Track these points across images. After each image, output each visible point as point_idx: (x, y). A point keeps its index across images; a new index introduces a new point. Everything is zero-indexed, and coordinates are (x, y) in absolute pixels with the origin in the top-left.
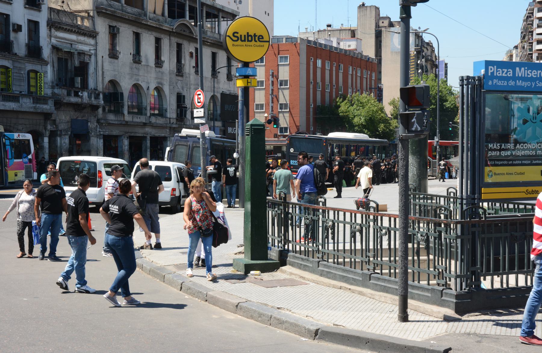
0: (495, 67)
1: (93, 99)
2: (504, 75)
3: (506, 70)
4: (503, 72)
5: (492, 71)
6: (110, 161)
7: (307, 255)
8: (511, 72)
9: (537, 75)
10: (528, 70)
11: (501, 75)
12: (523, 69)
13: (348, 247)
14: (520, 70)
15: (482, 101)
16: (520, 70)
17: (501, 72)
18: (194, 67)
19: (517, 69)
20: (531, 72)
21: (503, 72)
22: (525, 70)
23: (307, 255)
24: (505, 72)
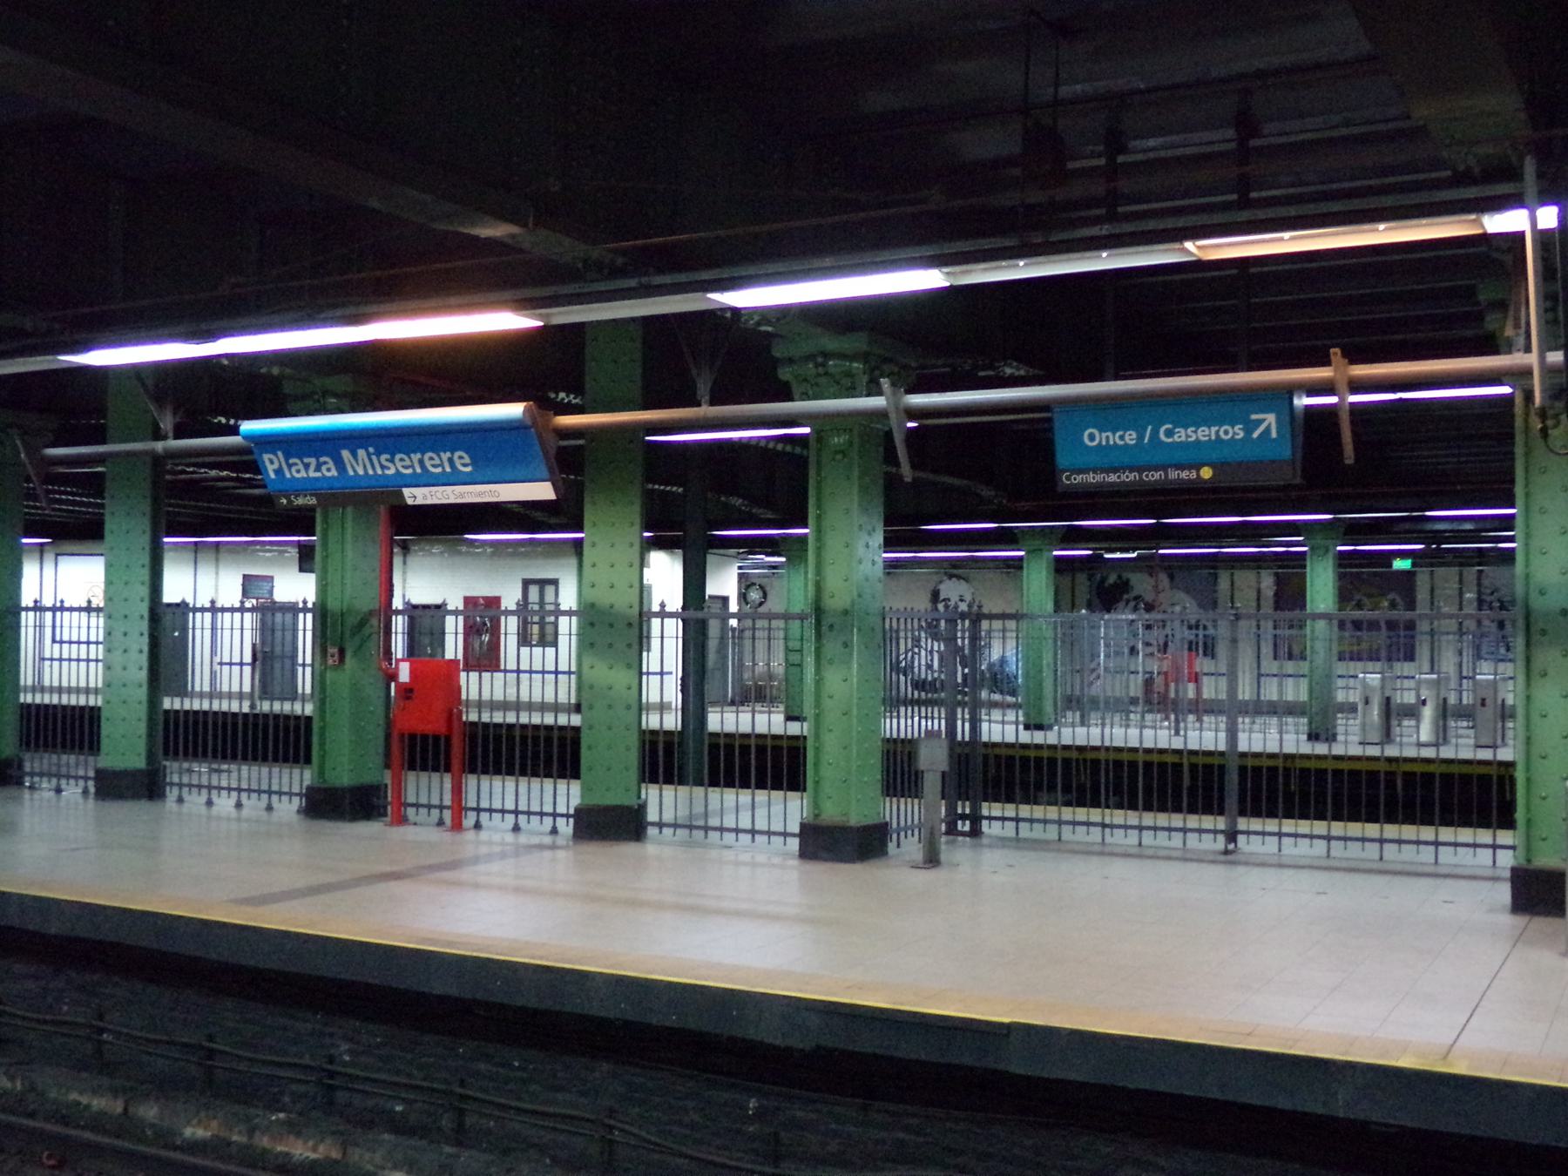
0: (280, 453)
1: (901, 1135)
2: (312, 474)
3: (313, 461)
4: (307, 466)
5: (276, 466)
6: (578, 312)
7: (992, 761)
8: (331, 464)
9: (412, 466)
10: (378, 454)
11: (303, 474)
12: (361, 453)
13: (902, 678)
14: (355, 455)
15: (1152, 225)
16: (355, 455)
17: (301, 467)
18: (89, 602)
19: (345, 454)
20: (392, 461)
21: (307, 466)
22: (369, 455)
23: (992, 761)
24: (312, 467)
